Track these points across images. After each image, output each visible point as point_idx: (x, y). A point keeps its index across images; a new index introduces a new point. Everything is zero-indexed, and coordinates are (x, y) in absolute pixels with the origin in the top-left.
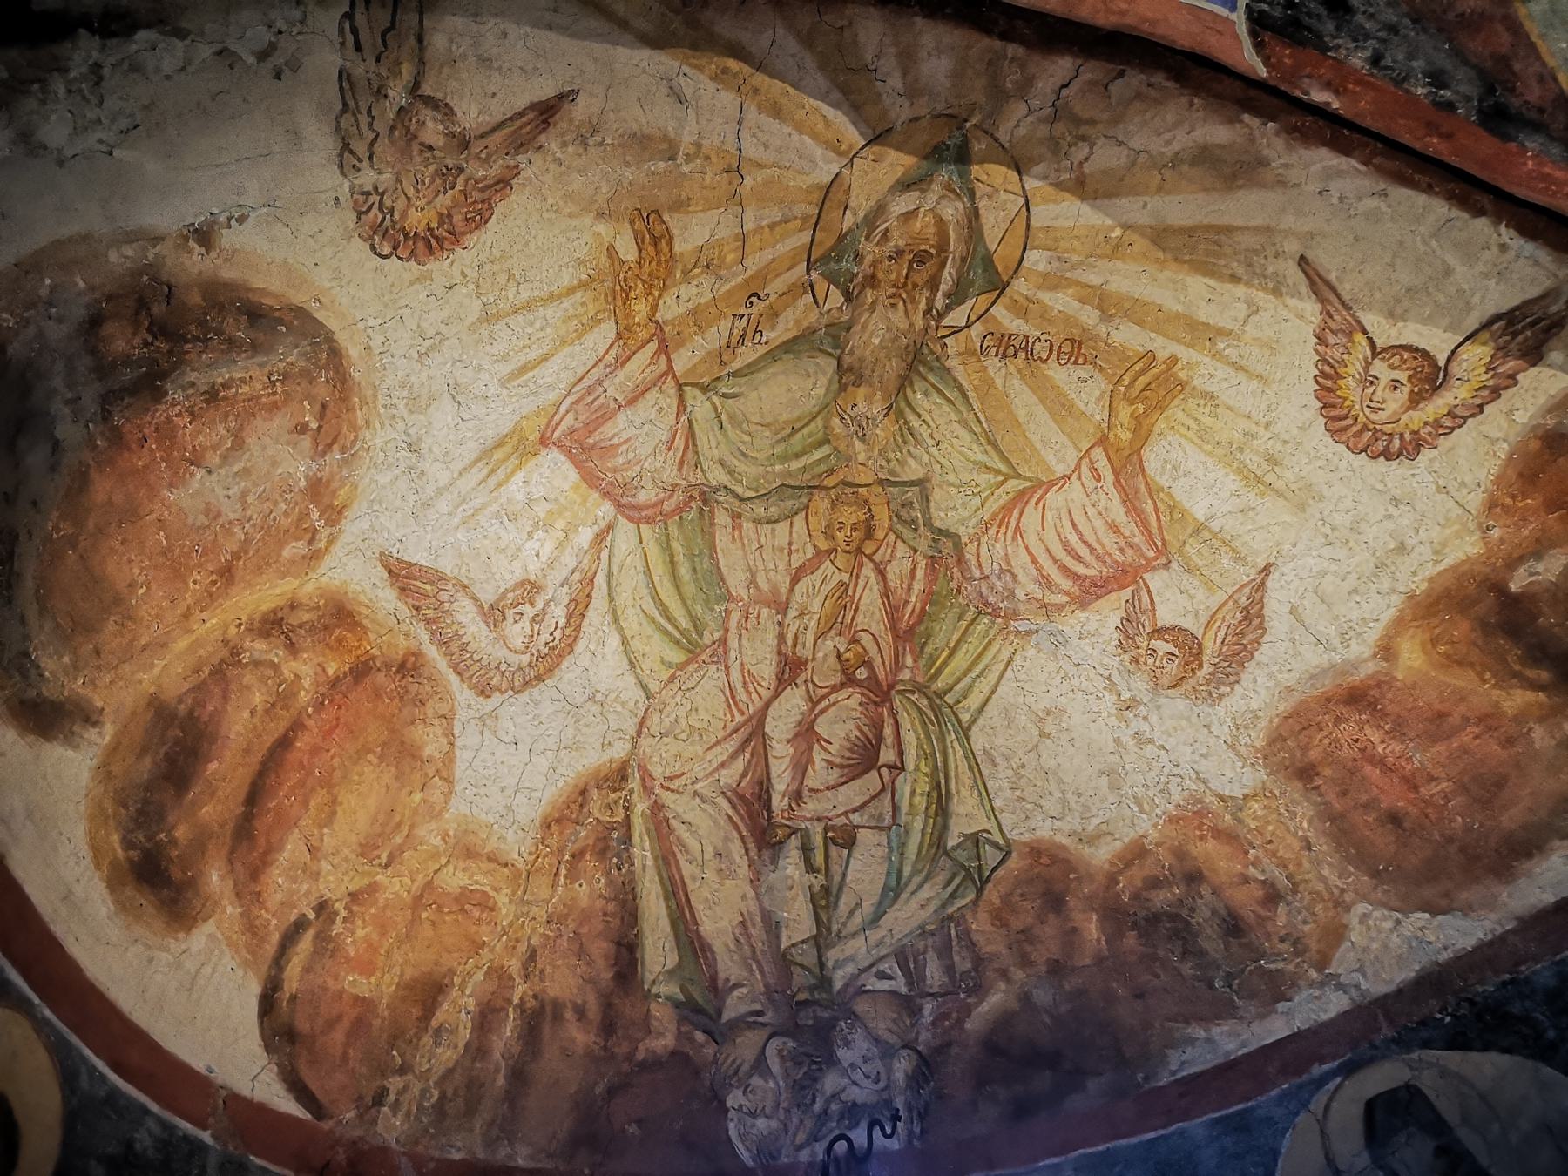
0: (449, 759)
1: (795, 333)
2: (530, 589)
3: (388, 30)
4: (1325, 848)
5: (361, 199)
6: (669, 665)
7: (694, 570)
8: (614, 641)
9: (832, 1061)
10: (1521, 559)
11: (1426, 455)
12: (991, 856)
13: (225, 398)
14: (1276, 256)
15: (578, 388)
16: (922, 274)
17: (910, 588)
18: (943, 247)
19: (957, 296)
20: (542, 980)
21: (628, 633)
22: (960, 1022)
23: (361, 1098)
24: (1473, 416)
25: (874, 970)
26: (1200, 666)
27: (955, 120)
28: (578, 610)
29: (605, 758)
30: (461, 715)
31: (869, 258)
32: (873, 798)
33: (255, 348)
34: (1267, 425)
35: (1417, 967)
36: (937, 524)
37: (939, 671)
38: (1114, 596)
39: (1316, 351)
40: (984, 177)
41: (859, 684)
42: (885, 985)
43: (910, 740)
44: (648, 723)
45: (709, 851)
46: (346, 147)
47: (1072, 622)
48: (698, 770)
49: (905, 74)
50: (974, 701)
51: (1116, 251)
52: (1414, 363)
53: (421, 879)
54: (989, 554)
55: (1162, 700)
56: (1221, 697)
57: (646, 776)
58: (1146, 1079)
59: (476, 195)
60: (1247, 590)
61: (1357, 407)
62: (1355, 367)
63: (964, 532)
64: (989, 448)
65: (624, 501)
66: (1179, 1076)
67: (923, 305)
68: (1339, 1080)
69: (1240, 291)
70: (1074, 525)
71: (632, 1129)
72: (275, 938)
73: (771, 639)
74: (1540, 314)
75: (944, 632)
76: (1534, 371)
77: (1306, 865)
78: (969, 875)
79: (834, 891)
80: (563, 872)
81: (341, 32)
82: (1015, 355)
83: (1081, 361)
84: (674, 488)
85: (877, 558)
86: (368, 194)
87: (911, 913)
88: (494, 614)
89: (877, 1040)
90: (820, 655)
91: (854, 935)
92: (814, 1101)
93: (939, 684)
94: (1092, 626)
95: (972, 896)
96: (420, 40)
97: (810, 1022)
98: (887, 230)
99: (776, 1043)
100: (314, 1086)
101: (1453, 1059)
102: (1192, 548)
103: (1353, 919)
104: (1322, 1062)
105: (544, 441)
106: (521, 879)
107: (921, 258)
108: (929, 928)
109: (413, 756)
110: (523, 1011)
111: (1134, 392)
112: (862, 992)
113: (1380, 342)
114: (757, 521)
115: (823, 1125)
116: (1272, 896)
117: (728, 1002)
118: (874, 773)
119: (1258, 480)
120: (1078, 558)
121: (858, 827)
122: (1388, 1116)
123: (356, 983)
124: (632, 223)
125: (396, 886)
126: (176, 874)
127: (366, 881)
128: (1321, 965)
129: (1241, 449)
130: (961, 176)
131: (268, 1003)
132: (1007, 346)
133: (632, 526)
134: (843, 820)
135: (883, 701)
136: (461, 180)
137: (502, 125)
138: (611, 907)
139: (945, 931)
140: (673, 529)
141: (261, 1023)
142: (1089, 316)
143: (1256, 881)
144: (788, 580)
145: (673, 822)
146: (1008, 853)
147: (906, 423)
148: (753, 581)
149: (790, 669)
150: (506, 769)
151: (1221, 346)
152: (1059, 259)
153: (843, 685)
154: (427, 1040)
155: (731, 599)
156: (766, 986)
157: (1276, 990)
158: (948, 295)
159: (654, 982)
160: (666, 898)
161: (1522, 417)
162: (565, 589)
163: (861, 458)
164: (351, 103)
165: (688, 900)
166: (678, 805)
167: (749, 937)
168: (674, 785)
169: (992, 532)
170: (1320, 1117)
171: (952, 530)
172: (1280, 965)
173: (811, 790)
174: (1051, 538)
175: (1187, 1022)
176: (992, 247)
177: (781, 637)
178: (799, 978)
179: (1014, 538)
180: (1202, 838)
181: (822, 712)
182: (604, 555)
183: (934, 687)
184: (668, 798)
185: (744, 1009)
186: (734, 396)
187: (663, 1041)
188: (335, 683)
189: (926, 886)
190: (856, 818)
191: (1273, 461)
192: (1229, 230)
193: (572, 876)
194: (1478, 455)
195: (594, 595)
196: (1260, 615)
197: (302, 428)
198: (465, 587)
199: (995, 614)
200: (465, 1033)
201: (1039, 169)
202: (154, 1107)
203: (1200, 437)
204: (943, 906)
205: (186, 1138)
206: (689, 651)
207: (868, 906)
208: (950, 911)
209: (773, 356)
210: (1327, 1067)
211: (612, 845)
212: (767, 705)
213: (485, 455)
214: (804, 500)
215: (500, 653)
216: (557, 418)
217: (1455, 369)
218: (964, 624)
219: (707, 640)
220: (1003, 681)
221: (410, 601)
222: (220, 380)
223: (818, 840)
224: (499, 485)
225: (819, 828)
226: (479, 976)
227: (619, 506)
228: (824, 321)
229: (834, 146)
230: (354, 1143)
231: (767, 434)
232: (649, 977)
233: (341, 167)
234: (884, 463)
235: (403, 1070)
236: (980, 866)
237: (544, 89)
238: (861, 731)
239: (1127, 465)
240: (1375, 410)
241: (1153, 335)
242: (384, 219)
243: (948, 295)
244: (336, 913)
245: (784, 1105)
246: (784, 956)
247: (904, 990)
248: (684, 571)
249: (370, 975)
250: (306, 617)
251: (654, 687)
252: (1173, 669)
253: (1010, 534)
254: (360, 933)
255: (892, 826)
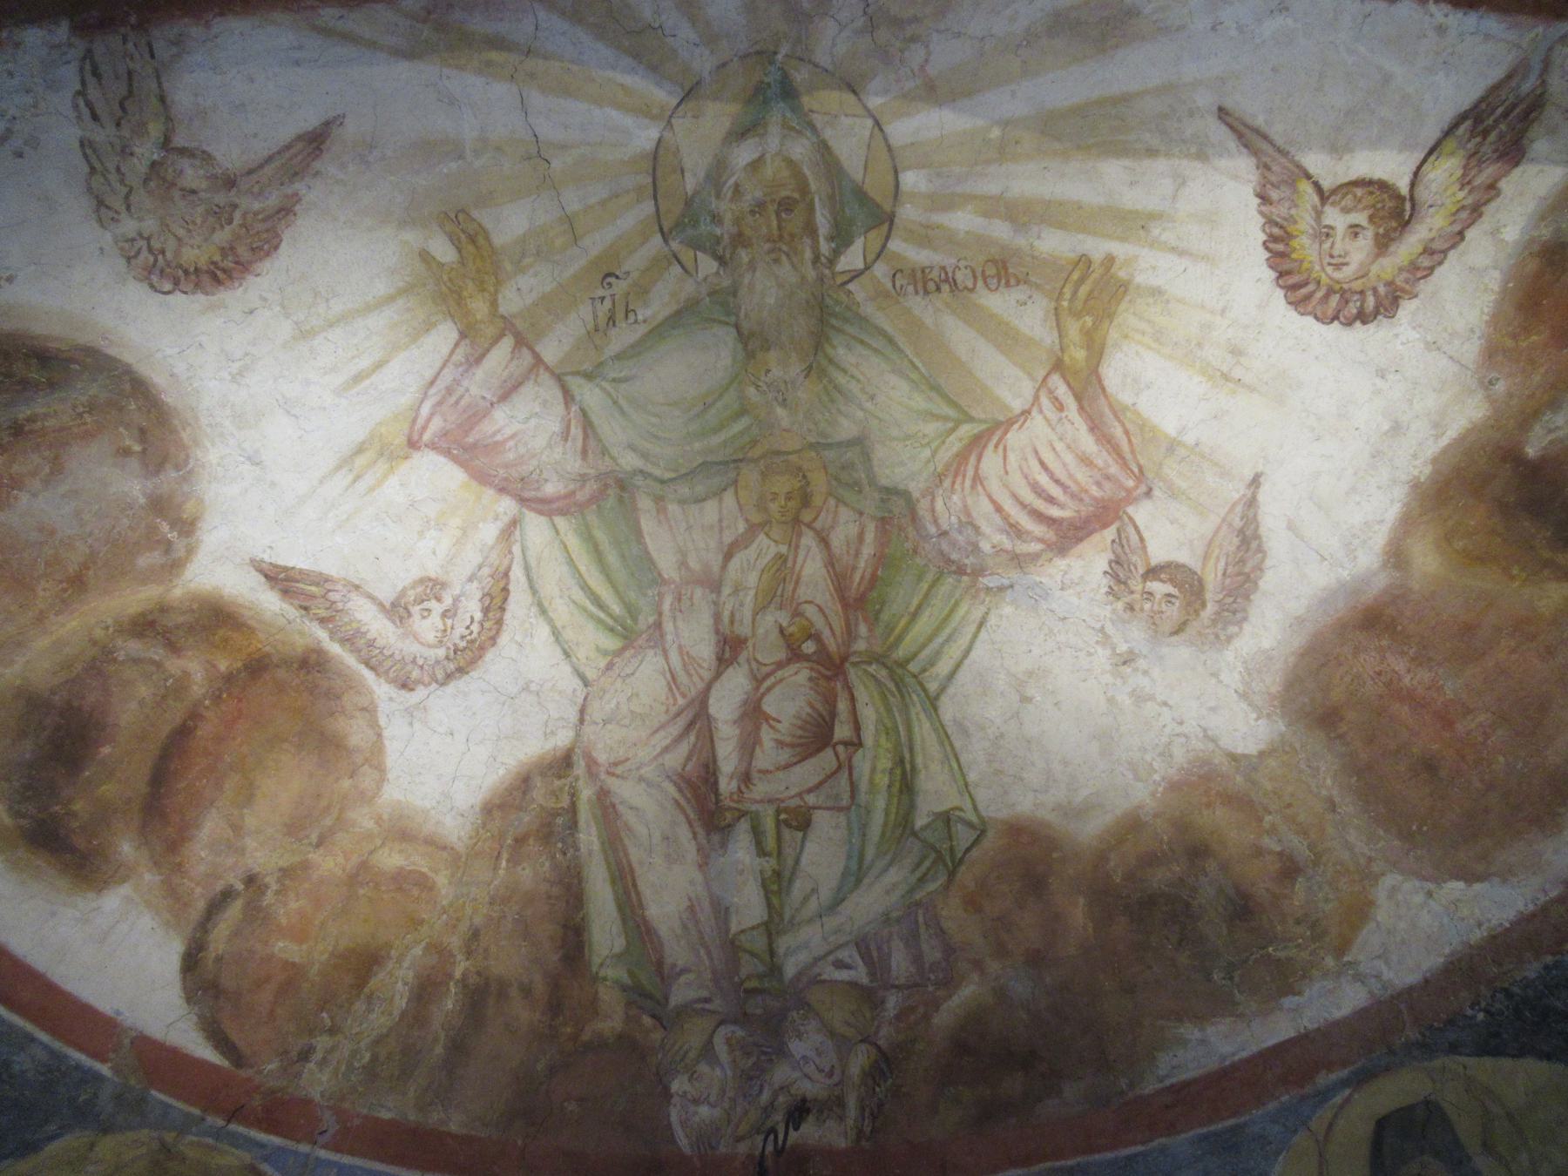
0: (378, 748)
1: (675, 307)
2: (432, 587)
3: (125, 98)
4: (1351, 809)
5: (127, 246)
6: (605, 653)
7: (623, 556)
8: (544, 631)
9: (782, 1052)
10: (1536, 414)
11: (1407, 308)
12: (963, 837)
13: (31, 432)
14: (1191, 114)
15: (432, 391)
16: (795, 222)
17: (857, 554)
18: (804, 188)
19: (842, 237)
20: (485, 958)
21: (559, 624)
22: (927, 1017)
23: (286, 1052)
24: (1453, 247)
25: (831, 958)
26: (1204, 605)
27: (764, 56)
28: (496, 603)
29: (549, 746)
30: (384, 708)
31: (728, 218)
32: (829, 777)
33: (52, 385)
34: (1223, 311)
35: (1447, 951)
36: (884, 482)
37: (900, 639)
38: (1096, 537)
39: (1261, 213)
40: (815, 107)
41: (807, 658)
42: (843, 975)
43: (868, 715)
44: (589, 711)
45: (657, 836)
46: (101, 203)
47: (1055, 571)
48: (644, 754)
49: (693, 21)
50: (943, 667)
51: (1003, 152)
52: (1370, 200)
53: (355, 860)
54: (946, 508)
55: (1165, 650)
56: (1229, 639)
57: (591, 763)
58: (1131, 1086)
59: (260, 227)
60: (1239, 509)
61: (1317, 268)
62: (1305, 222)
63: (915, 488)
64: (933, 394)
65: (527, 494)
66: (1168, 1083)
67: (808, 254)
68: (1347, 1092)
69: (1161, 164)
70: (1042, 464)
71: (571, 1106)
72: (201, 905)
73: (706, 619)
74: (1512, 99)
75: (901, 597)
76: (1517, 172)
77: (1330, 830)
78: (940, 858)
79: (787, 874)
80: (505, 856)
81: (76, 107)
82: (938, 289)
83: (1013, 281)
84: (583, 478)
85: (818, 525)
86: (133, 240)
87: (871, 902)
88: (397, 611)
89: (832, 1034)
90: (761, 631)
91: (810, 921)
92: (761, 1091)
93: (900, 653)
94: (1076, 573)
95: (942, 879)
96: (162, 99)
97: (759, 1011)
98: (737, 185)
99: (723, 1031)
100: (234, 1037)
101: (1484, 1068)
102: (1171, 470)
103: (1381, 893)
104: (1330, 1067)
105: (413, 444)
106: (457, 861)
107: (786, 206)
108: (894, 915)
109: (338, 746)
110: (465, 986)
111: (1079, 305)
112: (817, 981)
113: (1326, 184)
114: (682, 502)
115: (768, 1117)
116: (1290, 870)
117: (674, 988)
118: (829, 752)
119: (1226, 377)
120: (1051, 500)
121: (814, 808)
122: (1399, 1135)
123: (285, 949)
124: (441, 226)
125: (329, 864)
126: (80, 842)
127: (297, 859)
128: (1340, 951)
129: (1199, 345)
130: (793, 111)
131: (191, 962)
132: (926, 282)
133: (543, 520)
134: (795, 802)
135: (836, 675)
136: (237, 215)
137: (270, 159)
138: (556, 891)
139: (913, 916)
140: (592, 518)
141: (184, 980)
142: (1000, 231)
143: (1270, 852)
144: (720, 558)
145: (620, 808)
146: (983, 832)
147: (831, 381)
148: (683, 564)
149: (730, 648)
150: (440, 760)
151: (1156, 232)
152: (938, 175)
153: (789, 661)
154: (360, 1006)
155: (664, 582)
156: (714, 972)
157: (1285, 980)
158: (831, 238)
159: (601, 965)
160: (613, 882)
161: (1512, 233)
162: (475, 584)
163: (785, 423)
164: (97, 165)
165: (635, 885)
166: (627, 792)
167: (697, 922)
168: (619, 770)
169: (947, 483)
170: (1321, 1138)
171: (901, 487)
172: (1293, 952)
173: (760, 771)
174: (1017, 481)
175: (1180, 1020)
176: (858, 177)
177: (717, 617)
178: (748, 966)
179: (973, 487)
180: (1209, 805)
181: (769, 689)
182: (516, 549)
183: (894, 656)
184: (613, 784)
185: (692, 994)
186: (626, 380)
187: (611, 1020)
188: (229, 678)
189: (893, 871)
190: (811, 799)
191: (1236, 352)
192: (1126, 99)
193: (514, 861)
194: (1464, 296)
195: (511, 587)
196: (1257, 537)
197: (126, 452)
198: (357, 587)
199: (961, 571)
200: (401, 1003)
201: (875, 84)
202: (44, 1037)
203: (1157, 340)
204: (911, 891)
205: (78, 1067)
206: (625, 638)
207: (826, 894)
208: (917, 897)
209: (659, 332)
210: (1333, 1077)
211: (556, 829)
212: (709, 688)
213: (346, 462)
214: (732, 475)
215: (411, 648)
216: (420, 422)
217: (1423, 194)
218: (925, 586)
219: (642, 625)
220: (978, 644)
221: (296, 602)
222: (21, 416)
223: (769, 824)
224: (372, 489)
225: (771, 810)
226: (418, 951)
227: (523, 501)
228: (704, 290)
229: (645, 111)
230: (273, 1092)
231: (677, 413)
232: (596, 960)
233: (100, 220)
234: (812, 427)
235: (333, 1031)
236: (952, 849)
237: (309, 120)
238: (812, 707)
239: (1087, 386)
240: (1338, 267)
241: (1080, 236)
242: (156, 261)
243: (831, 238)
244: (267, 887)
245: (731, 1094)
246: (732, 942)
247: (865, 980)
248: (612, 558)
249: (302, 940)
250: (181, 619)
251: (591, 674)
252: (1174, 612)
253: (968, 483)
254: (293, 905)
255: (852, 806)
